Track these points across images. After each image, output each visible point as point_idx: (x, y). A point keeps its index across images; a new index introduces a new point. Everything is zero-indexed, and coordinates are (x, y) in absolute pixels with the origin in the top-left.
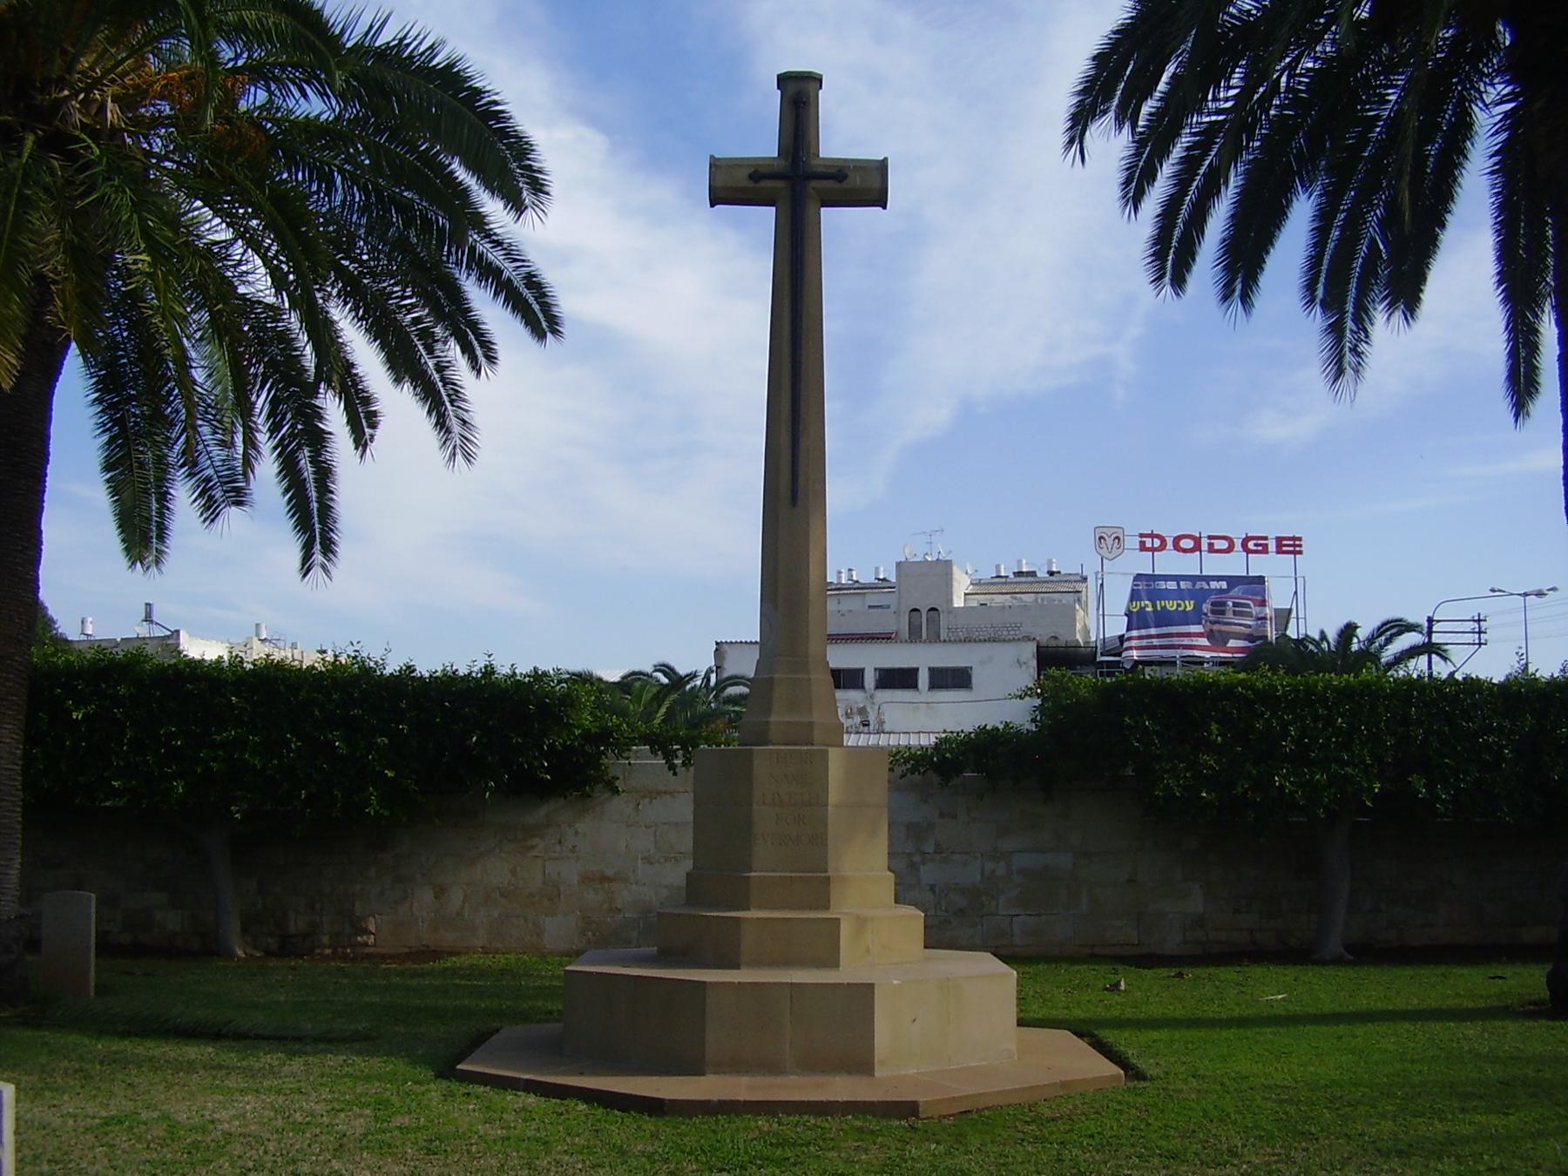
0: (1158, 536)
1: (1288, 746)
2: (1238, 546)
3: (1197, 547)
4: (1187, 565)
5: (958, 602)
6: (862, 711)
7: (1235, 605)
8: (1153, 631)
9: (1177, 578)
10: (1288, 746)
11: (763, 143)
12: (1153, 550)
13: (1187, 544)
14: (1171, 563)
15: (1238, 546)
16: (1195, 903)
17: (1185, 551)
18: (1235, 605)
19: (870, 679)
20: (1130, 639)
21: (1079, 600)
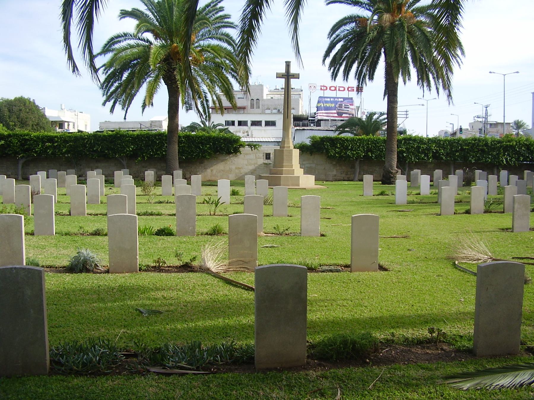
0: (325, 86)
1: (350, 148)
2: (346, 89)
3: (335, 89)
4: (332, 94)
5: (265, 97)
6: (247, 132)
7: (345, 105)
8: (323, 112)
9: (330, 98)
10: (350, 148)
11: (283, 71)
12: (324, 90)
13: (333, 88)
14: (329, 94)
15: (346, 89)
16: (335, 173)
17: (332, 90)
18: (345, 105)
19: (249, 123)
20: (318, 113)
21: (300, 97)
